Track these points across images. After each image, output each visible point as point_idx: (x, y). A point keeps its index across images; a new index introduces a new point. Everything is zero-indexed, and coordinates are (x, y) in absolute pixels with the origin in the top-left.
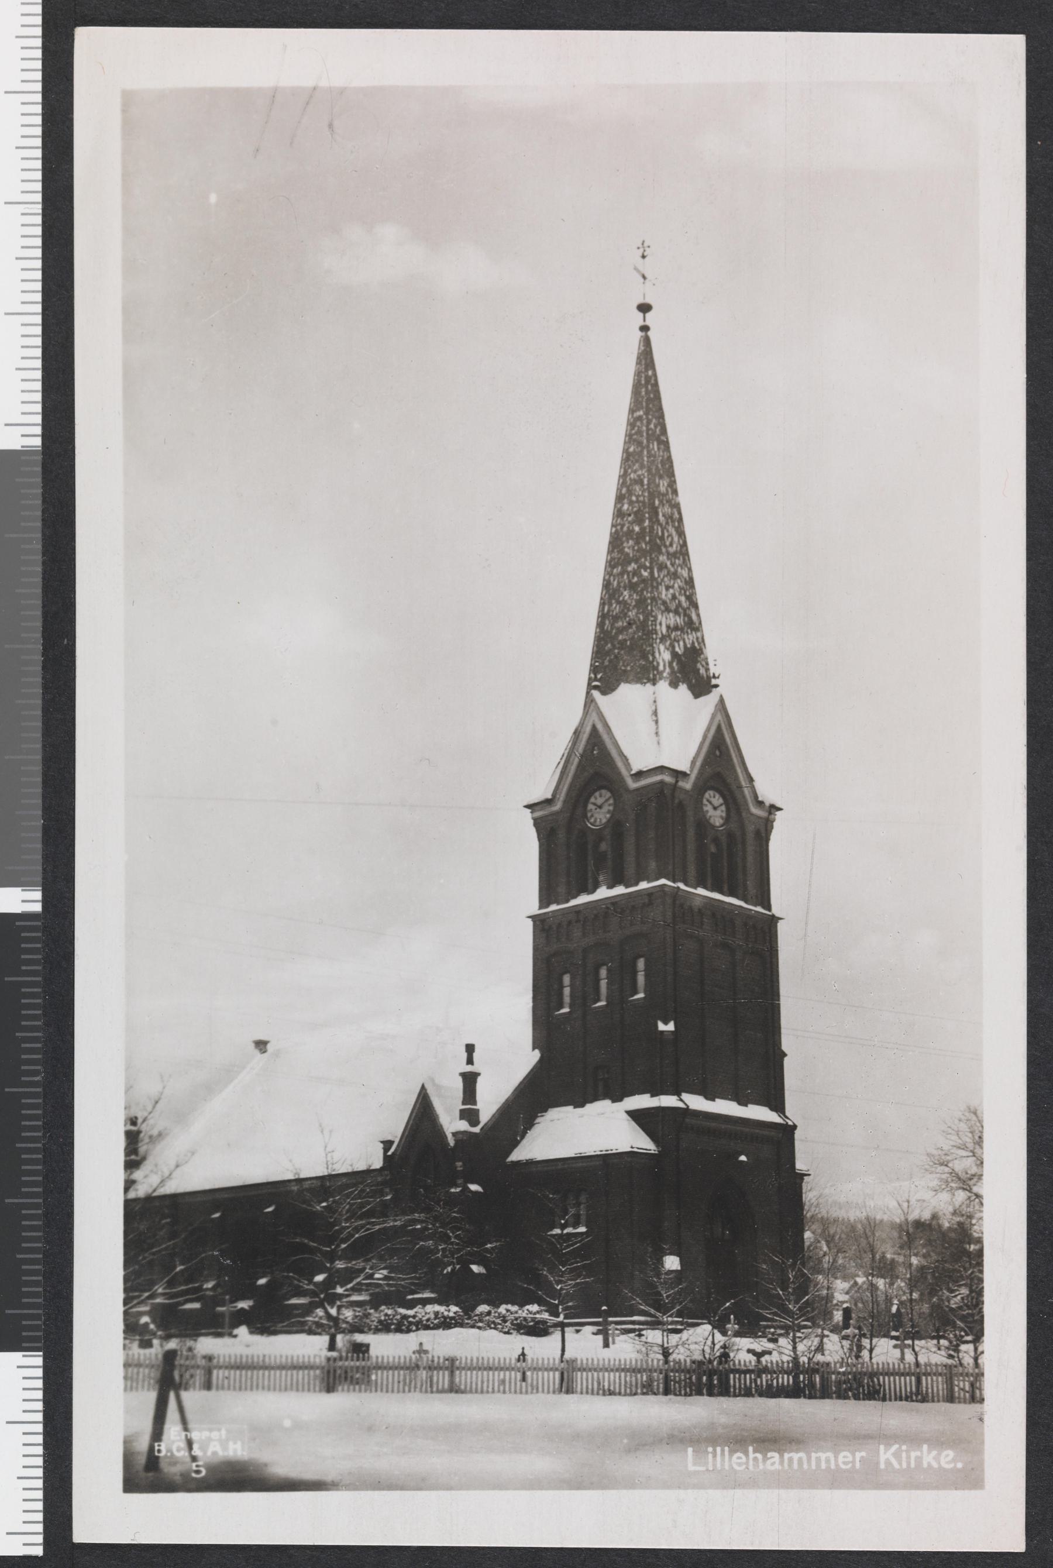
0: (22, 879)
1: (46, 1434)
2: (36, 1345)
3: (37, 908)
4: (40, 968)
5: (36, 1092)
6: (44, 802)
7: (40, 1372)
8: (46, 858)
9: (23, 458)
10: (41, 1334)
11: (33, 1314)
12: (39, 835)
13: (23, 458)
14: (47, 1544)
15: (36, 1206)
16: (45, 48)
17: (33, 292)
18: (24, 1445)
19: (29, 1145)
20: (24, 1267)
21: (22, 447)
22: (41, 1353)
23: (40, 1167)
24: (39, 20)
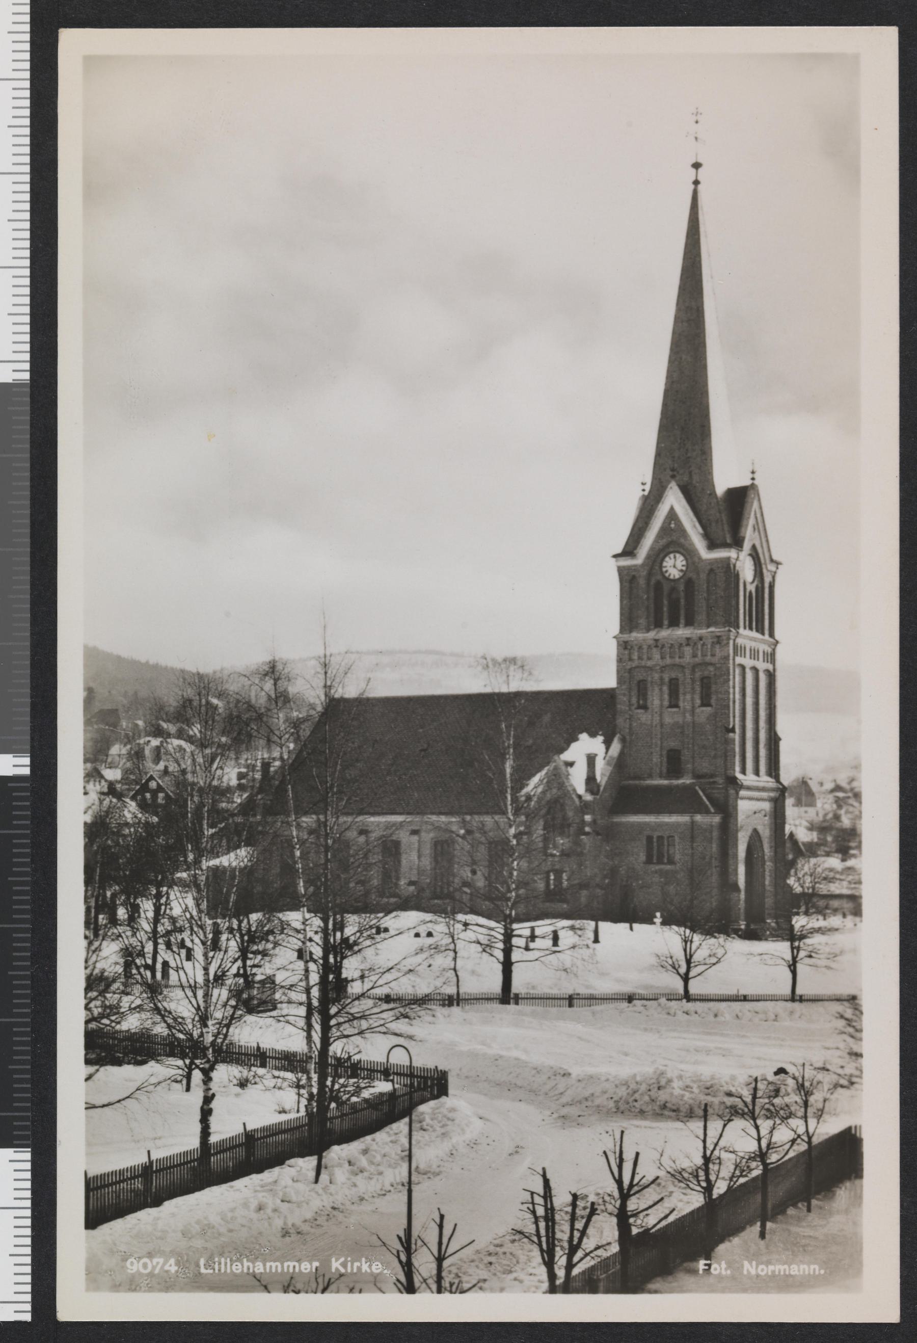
0: (14, 747)
1: (34, 1218)
2: (25, 1142)
3: (26, 771)
4: (28, 822)
5: (26, 1126)
6: (31, 682)
7: (28, 1166)
8: (33, 730)
9: (14, 390)
10: (29, 1133)
11: (23, 1116)
12: (28, 709)
13: (14, 390)
14: (34, 1311)
15: (25, 1025)
16: (33, 42)
17: (23, 249)
18: (14, 61)
19: (19, 973)
20: (15, 1076)
21: (14, 380)
22: (30, 1149)
23: (29, 992)
24: (27, 18)
